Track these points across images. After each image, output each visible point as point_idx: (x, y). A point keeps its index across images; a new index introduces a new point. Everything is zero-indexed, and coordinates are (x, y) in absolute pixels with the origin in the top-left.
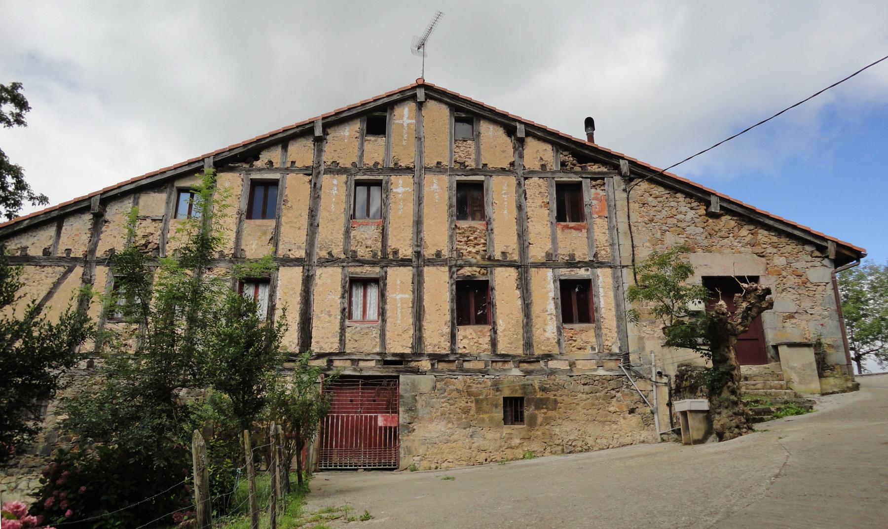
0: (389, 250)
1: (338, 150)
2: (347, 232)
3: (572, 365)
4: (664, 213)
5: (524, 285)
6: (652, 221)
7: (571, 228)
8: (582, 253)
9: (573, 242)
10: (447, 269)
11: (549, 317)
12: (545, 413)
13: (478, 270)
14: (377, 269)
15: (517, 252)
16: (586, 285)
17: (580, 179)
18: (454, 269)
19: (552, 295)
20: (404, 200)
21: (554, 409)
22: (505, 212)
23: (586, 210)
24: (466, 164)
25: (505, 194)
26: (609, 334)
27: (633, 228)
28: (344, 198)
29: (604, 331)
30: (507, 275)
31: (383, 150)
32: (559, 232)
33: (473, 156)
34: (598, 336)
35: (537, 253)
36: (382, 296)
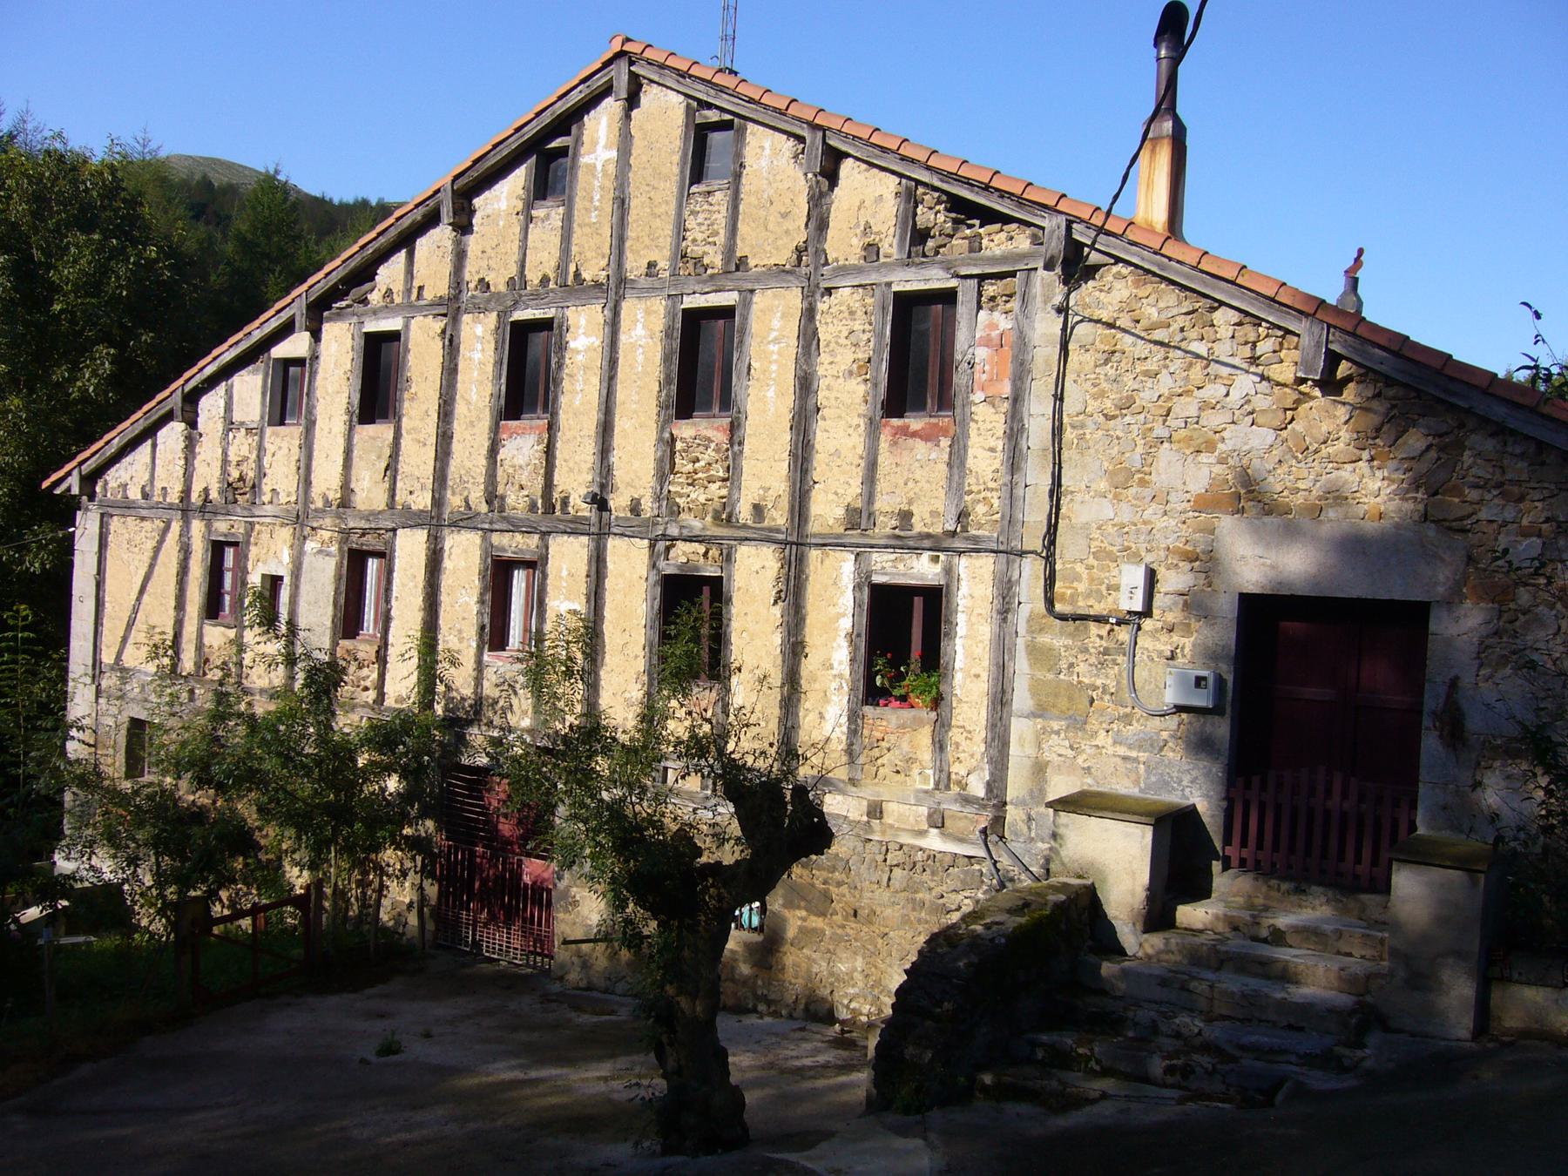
0: (556, 495)
1: (489, 250)
2: (493, 451)
3: (876, 811)
4: (1165, 384)
5: (792, 592)
6: (1126, 405)
7: (914, 434)
8: (932, 514)
9: (915, 475)
10: (646, 542)
11: (834, 685)
12: (804, 919)
13: (701, 549)
14: (534, 541)
15: (785, 503)
16: (935, 600)
17: (953, 283)
18: (661, 545)
19: (846, 624)
20: (586, 368)
21: (823, 914)
22: (771, 394)
23: (960, 379)
24: (706, 261)
25: (776, 341)
26: (964, 745)
27: (1069, 435)
28: (490, 368)
29: (955, 735)
30: (757, 567)
31: (557, 241)
32: (884, 444)
33: (721, 239)
34: (940, 746)
35: (826, 510)
36: (389, 573)
